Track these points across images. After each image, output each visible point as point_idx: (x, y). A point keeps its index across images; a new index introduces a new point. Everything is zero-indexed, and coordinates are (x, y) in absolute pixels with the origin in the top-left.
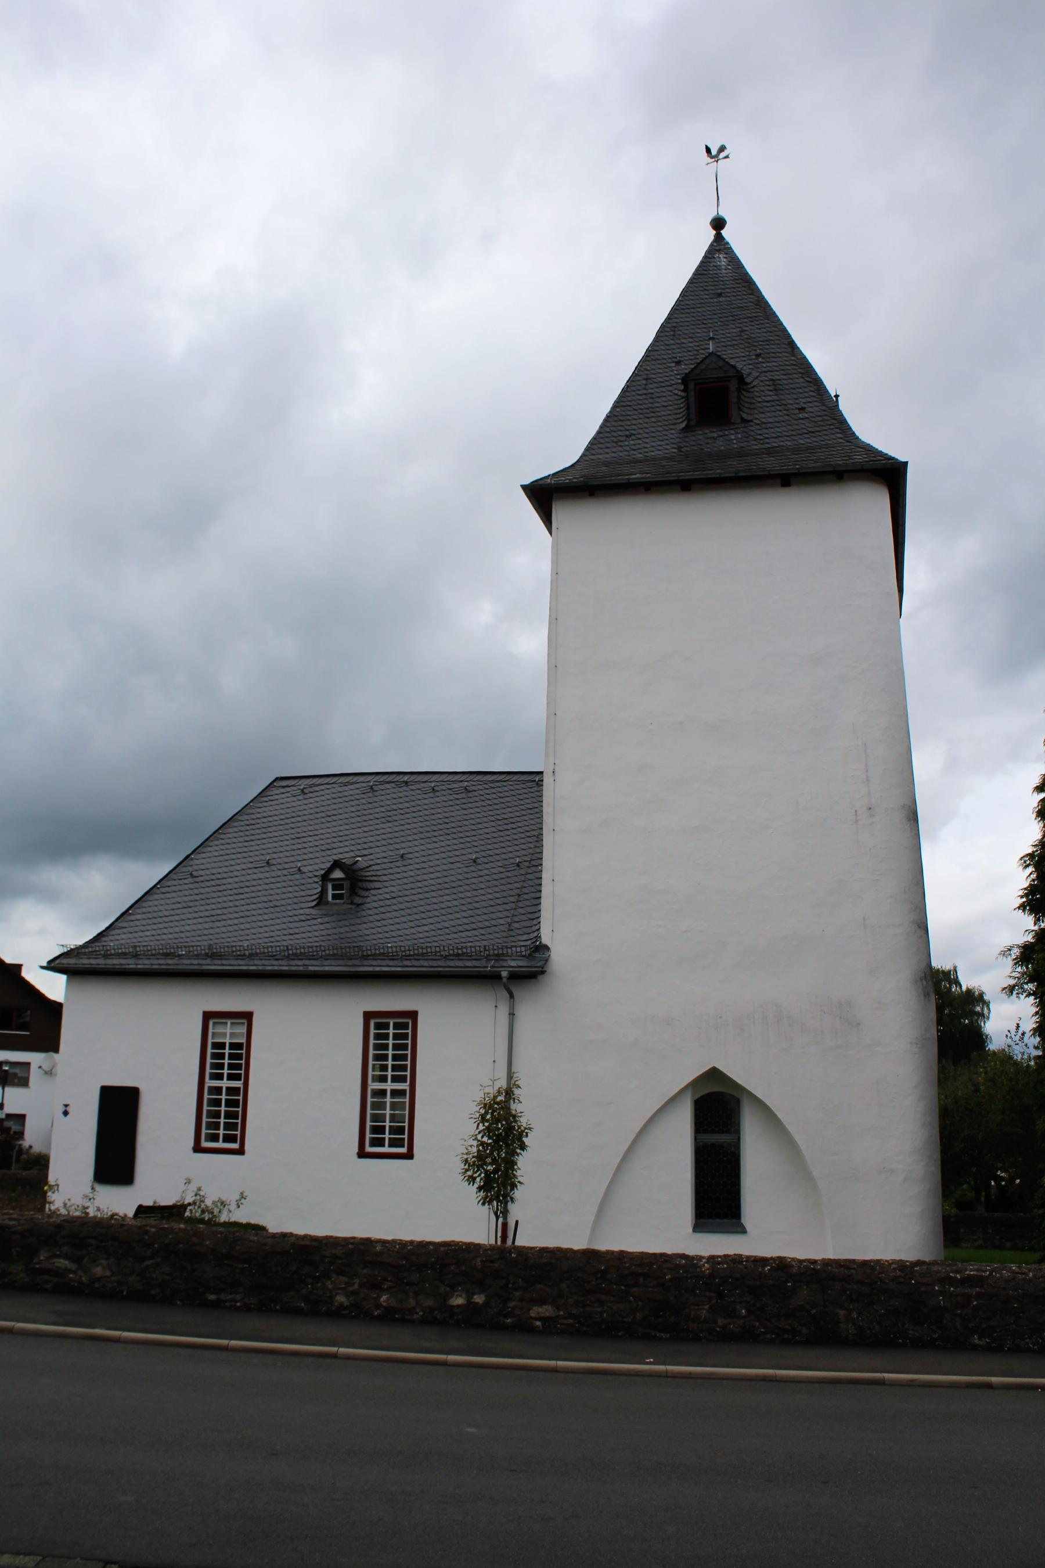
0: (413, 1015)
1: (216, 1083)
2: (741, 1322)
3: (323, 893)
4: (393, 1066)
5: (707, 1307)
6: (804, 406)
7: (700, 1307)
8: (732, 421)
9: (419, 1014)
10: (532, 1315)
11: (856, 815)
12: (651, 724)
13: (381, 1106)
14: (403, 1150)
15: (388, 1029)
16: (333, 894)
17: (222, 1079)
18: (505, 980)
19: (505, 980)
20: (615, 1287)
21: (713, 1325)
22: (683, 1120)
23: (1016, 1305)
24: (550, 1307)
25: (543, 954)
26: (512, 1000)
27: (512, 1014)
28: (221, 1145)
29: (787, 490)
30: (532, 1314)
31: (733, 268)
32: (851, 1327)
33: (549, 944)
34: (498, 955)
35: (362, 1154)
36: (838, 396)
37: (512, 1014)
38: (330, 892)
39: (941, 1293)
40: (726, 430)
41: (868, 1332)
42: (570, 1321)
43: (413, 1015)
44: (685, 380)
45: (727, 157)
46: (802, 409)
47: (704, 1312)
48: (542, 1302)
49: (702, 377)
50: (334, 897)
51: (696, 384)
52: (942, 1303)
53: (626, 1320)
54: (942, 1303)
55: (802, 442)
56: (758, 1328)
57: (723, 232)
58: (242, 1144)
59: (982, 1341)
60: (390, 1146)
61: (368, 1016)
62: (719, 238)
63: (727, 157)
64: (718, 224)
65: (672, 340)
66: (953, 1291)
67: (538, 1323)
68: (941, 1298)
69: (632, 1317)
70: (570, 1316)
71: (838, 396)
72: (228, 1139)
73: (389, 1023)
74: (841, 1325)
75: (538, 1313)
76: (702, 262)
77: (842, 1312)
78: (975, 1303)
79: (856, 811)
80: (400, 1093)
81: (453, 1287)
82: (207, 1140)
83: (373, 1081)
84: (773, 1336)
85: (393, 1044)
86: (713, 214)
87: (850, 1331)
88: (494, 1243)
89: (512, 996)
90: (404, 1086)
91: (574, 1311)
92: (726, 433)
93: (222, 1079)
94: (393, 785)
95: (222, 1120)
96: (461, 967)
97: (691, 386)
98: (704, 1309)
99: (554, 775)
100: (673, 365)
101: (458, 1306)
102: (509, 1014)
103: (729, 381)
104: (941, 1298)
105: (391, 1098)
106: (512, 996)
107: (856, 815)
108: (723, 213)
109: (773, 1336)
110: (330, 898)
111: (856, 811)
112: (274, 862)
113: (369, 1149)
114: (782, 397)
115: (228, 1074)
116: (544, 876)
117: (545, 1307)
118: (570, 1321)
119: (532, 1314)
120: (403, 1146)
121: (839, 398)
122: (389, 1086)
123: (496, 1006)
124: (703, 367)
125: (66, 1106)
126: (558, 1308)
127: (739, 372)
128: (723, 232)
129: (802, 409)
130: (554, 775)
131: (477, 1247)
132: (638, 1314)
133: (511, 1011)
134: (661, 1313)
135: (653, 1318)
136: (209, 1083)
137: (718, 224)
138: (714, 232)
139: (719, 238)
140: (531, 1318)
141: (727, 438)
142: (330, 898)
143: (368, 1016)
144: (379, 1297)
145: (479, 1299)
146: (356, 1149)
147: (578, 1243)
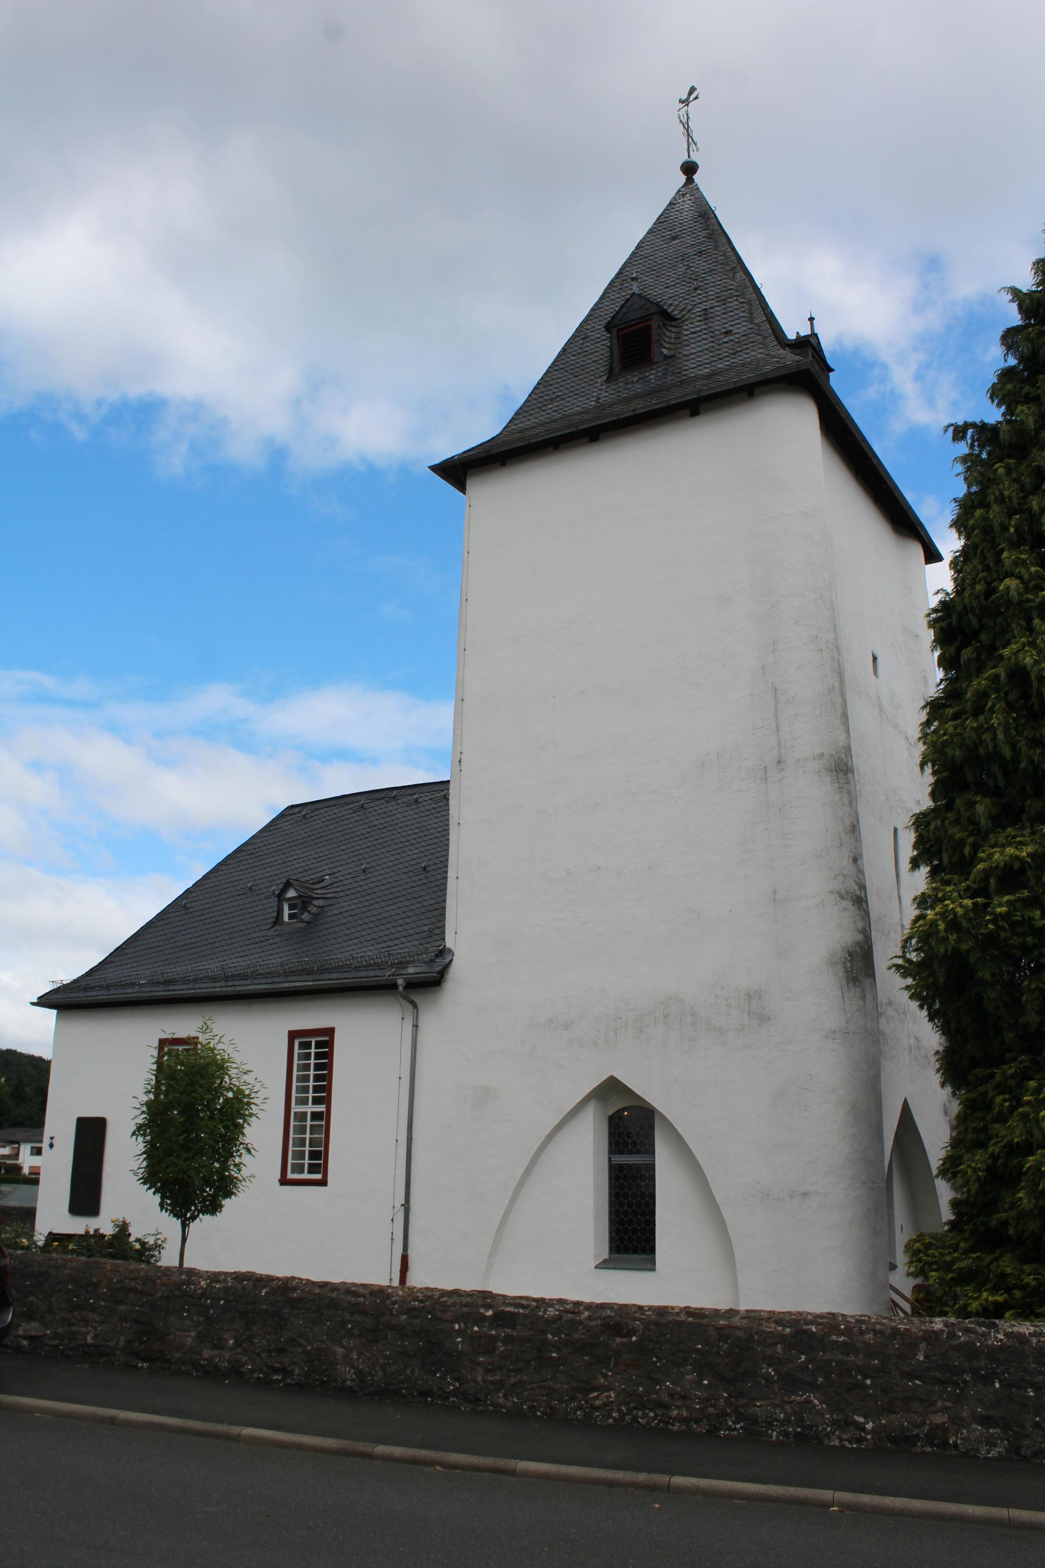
0: (330, 1032)
1: (301, 1109)
2: (227, 1355)
3: (280, 912)
5: (193, 1334)
6: (730, 328)
7: (186, 1334)
8: (655, 361)
9: (336, 1031)
10: (21, 1333)
11: (766, 771)
12: (554, 697)
13: (302, 1130)
16: (289, 914)
18: (401, 988)
19: (401, 988)
20: (102, 1303)
21: (198, 1357)
23: (554, 1355)
24: (37, 1325)
25: (444, 959)
26: (415, 1010)
27: (416, 1026)
28: (306, 1176)
29: (697, 420)
31: (695, 208)
32: (349, 1371)
33: (452, 948)
34: (401, 963)
36: (814, 319)
37: (416, 1026)
39: (460, 1332)
40: (647, 371)
41: (369, 1378)
43: (330, 1032)
44: (608, 328)
45: (697, 98)
46: (728, 333)
47: (190, 1339)
49: (625, 321)
50: (291, 916)
51: (619, 330)
52: (460, 1346)
53: (109, 1343)
54: (460, 1346)
55: (721, 366)
56: (245, 1363)
59: (508, 1400)
60: (310, 1172)
61: (293, 1035)
63: (697, 98)
64: (689, 169)
65: (619, 293)
66: (476, 1332)
67: (25, 1343)
68: (459, 1339)
69: (114, 1342)
71: (814, 319)
72: (313, 1169)
73: (311, 1042)
74: (339, 1367)
75: (26, 1331)
77: (340, 1350)
78: (502, 1349)
79: (765, 767)
82: (293, 1172)
83: (296, 1104)
84: (261, 1375)
85: (315, 1064)
86: (685, 158)
87: (348, 1376)
88: (396, 1283)
89: (415, 1006)
91: (60, 1331)
92: (647, 374)
94: (383, 801)
95: (307, 1161)
96: (351, 978)
97: (615, 332)
98: (190, 1336)
99: (460, 765)
100: (723, 336)
102: (413, 1026)
103: (651, 319)
104: (459, 1339)
105: (311, 1121)
106: (415, 1006)
107: (766, 771)
108: (695, 157)
109: (261, 1375)
110: (286, 918)
111: (765, 767)
112: (256, 888)
113: (291, 1176)
114: (711, 325)
116: (449, 874)
117: (32, 1324)
121: (814, 321)
123: (403, 1018)
124: (625, 310)
125: (52, 1138)
127: (657, 304)
129: (728, 333)
130: (460, 765)
132: (122, 1338)
133: (415, 1023)
134: (145, 1339)
135: (136, 1344)
137: (689, 169)
140: (20, 1336)
141: (646, 379)
142: (286, 918)
143: (293, 1035)
146: (279, 1177)
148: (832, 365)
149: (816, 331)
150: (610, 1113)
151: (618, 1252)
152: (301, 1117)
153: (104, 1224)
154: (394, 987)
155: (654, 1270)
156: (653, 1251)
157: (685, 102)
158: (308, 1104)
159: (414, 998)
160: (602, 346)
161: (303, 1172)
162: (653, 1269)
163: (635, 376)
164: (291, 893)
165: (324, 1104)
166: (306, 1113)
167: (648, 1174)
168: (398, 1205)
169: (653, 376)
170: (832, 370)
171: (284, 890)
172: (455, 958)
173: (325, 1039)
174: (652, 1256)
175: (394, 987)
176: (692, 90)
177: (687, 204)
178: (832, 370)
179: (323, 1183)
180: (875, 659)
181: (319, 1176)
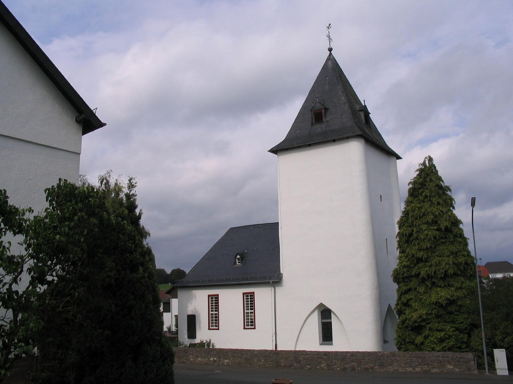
0: (253, 293)
3: (235, 262)
4: (215, 308)
14: (253, 327)
15: (250, 298)
17: (213, 311)
22: (316, 316)
28: (250, 327)
29: (335, 143)
30: (225, 361)
33: (282, 273)
35: (244, 328)
38: (237, 261)
42: (232, 363)
43: (253, 293)
45: (331, 27)
48: (226, 359)
57: (331, 52)
58: (255, 327)
62: (331, 54)
63: (331, 27)
64: (330, 50)
70: (231, 362)
72: (216, 326)
76: (324, 65)
80: (252, 312)
81: (211, 356)
82: (211, 327)
88: (274, 349)
90: (253, 311)
93: (213, 311)
101: (212, 360)
113: (246, 327)
115: (215, 310)
118: (232, 363)
119: (225, 361)
120: (253, 326)
122: (250, 311)
126: (229, 360)
128: (331, 52)
131: (292, 351)
136: (211, 313)
137: (330, 50)
138: (329, 52)
139: (331, 54)
143: (244, 294)
144: (198, 359)
145: (215, 359)
147: (292, 349)
148: (370, 113)
149: (365, 104)
150: (322, 310)
151: (324, 341)
152: (248, 313)
153: (197, 341)
154: (269, 283)
155: (332, 345)
156: (332, 341)
157: (328, 28)
158: (249, 310)
159: (317, 311)
160: (310, 116)
161: (249, 326)
162: (332, 345)
163: (319, 126)
164: (238, 257)
165: (493, 351)
166: (249, 312)
167: (330, 324)
168: (273, 333)
169: (323, 126)
170: (370, 114)
171: (236, 256)
172: (283, 276)
173: (252, 294)
174: (332, 342)
175: (269, 283)
176: (330, 25)
177: (330, 63)
178: (370, 114)
179: (218, 329)
180: (381, 196)
181: (217, 328)
